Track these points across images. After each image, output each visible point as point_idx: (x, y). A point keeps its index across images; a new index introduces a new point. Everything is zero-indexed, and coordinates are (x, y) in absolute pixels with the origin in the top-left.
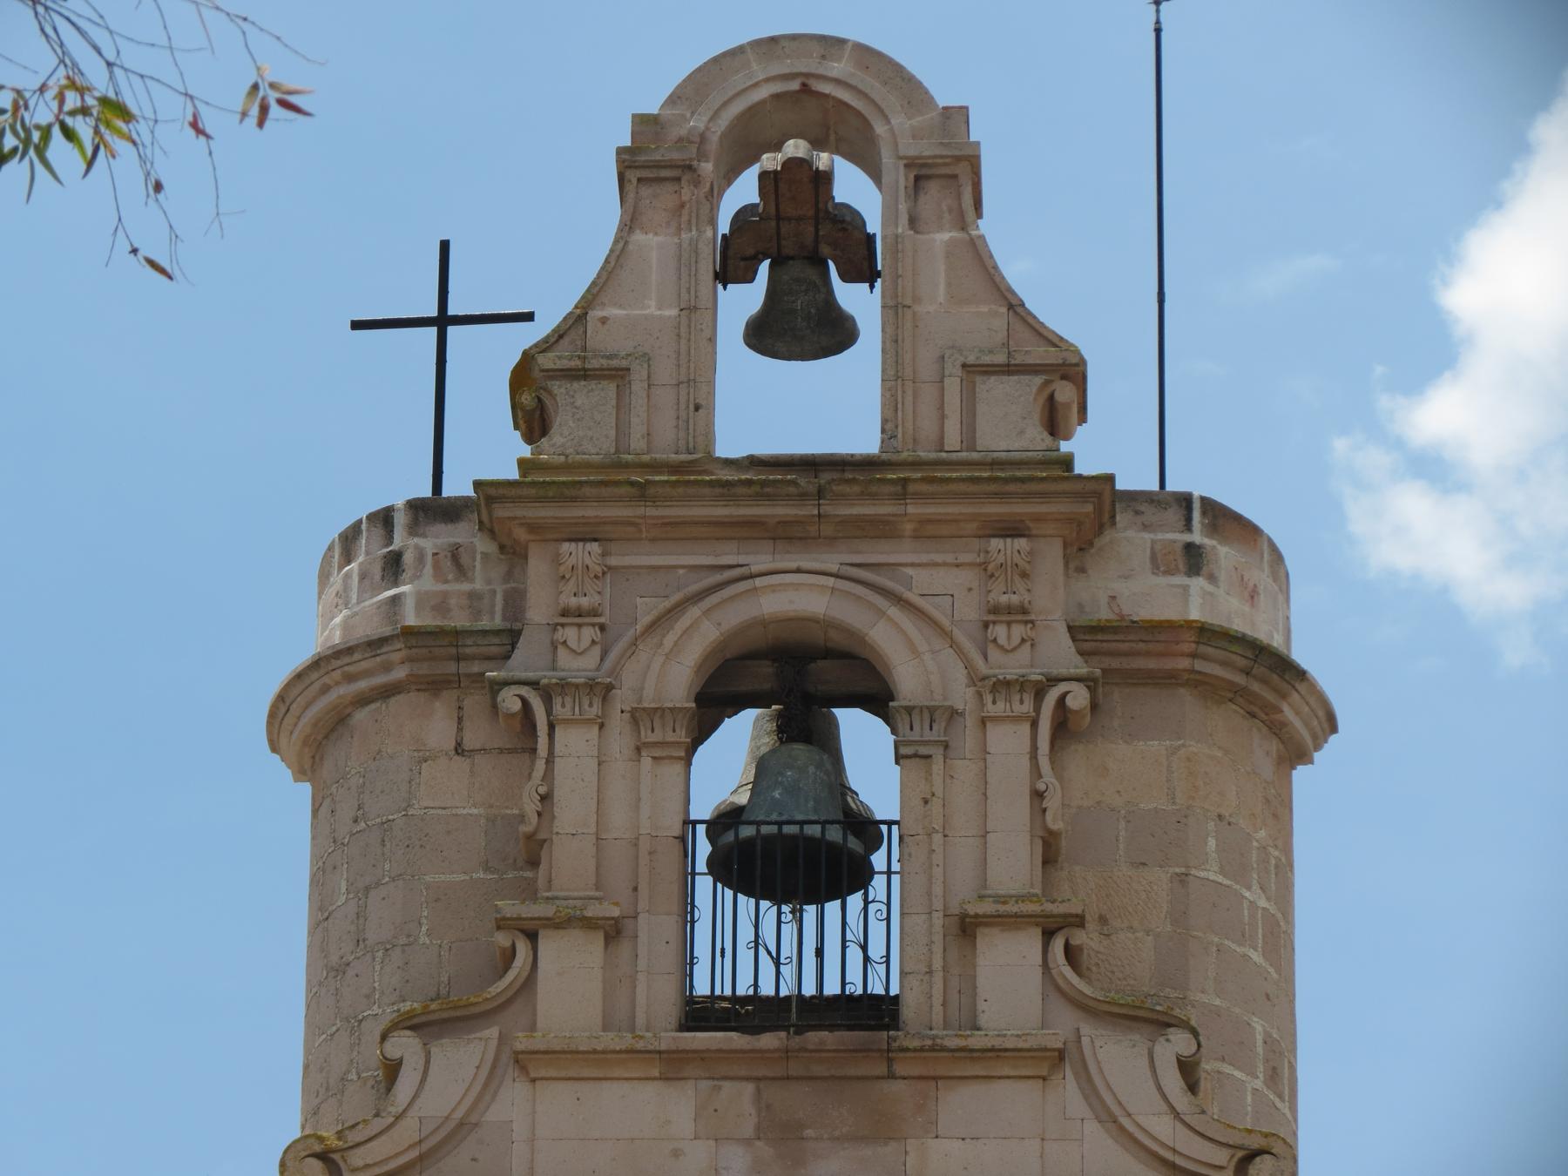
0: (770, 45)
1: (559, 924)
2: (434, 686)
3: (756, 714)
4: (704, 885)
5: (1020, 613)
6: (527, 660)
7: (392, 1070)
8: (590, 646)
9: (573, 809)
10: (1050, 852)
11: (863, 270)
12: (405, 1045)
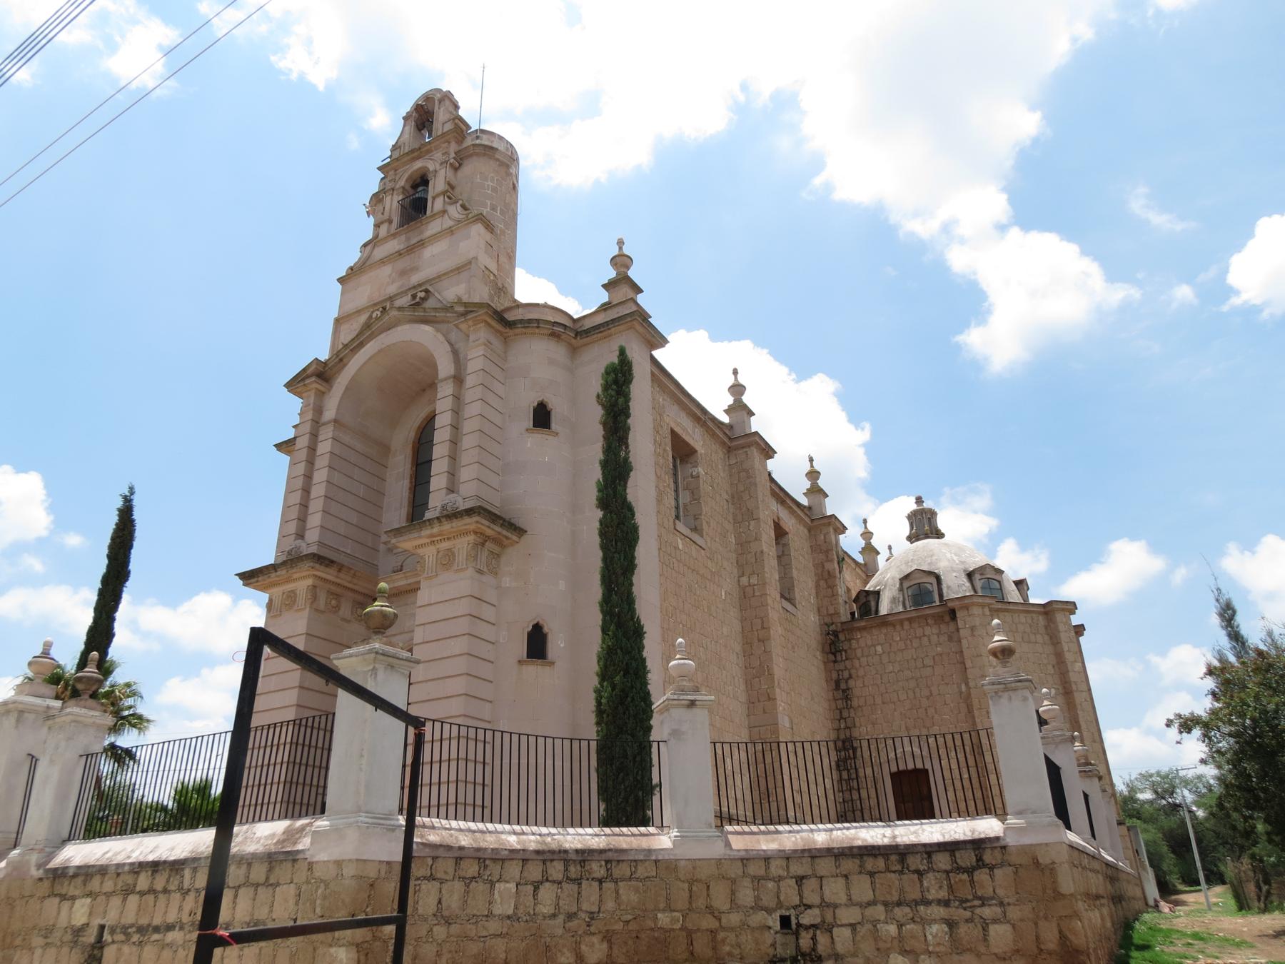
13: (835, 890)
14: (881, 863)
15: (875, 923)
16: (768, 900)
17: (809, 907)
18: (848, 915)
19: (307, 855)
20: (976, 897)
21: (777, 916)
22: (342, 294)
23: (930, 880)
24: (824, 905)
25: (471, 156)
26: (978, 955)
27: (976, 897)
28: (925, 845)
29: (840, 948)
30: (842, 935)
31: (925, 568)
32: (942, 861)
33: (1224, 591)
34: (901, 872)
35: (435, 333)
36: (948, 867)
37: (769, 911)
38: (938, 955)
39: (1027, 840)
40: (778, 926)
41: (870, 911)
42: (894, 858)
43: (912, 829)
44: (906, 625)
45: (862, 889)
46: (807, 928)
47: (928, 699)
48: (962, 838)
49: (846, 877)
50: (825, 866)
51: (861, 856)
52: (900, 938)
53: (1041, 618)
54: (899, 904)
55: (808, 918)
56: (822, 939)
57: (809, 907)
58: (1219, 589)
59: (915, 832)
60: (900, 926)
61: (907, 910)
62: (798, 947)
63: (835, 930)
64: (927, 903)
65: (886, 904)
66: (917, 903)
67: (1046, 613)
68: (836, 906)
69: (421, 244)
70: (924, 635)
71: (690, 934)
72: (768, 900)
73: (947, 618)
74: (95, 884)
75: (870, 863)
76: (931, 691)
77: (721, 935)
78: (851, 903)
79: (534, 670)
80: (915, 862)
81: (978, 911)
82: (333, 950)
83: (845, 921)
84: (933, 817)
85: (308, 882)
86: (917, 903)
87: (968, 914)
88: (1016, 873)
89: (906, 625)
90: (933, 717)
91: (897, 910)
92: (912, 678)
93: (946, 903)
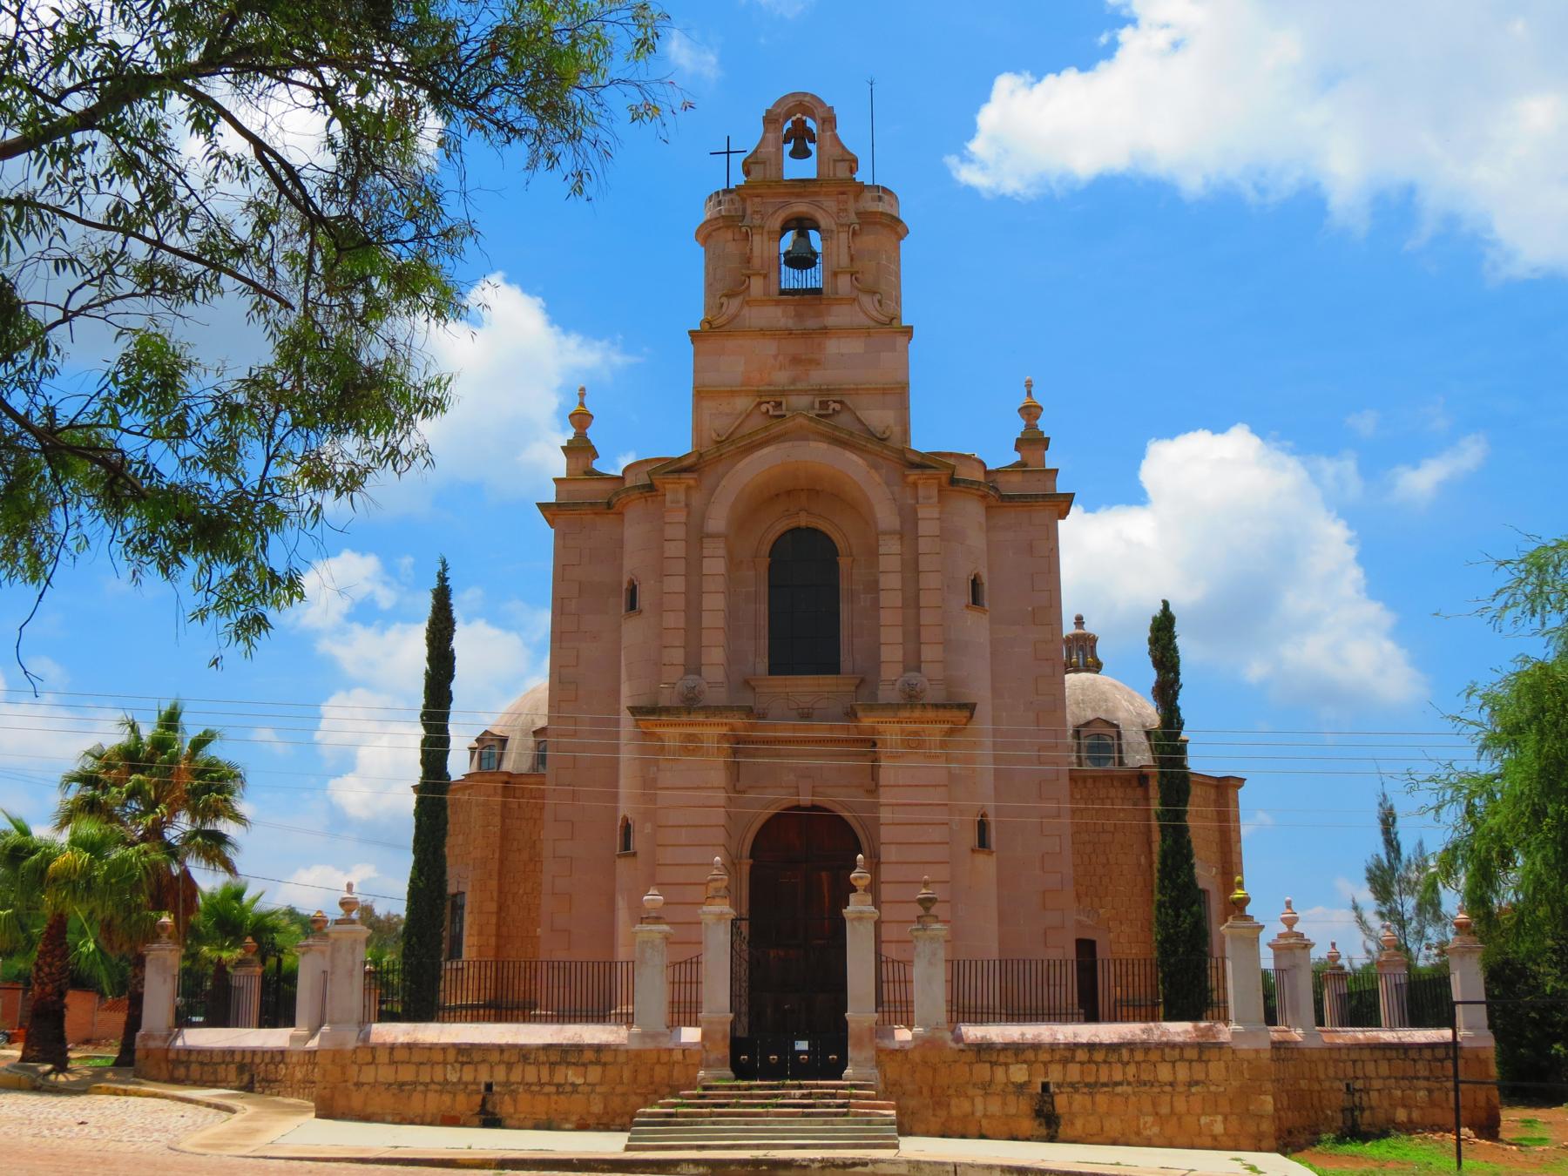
2: (728, 227)
6: (747, 221)
9: (757, 252)
11: (813, 141)
12: (724, 300)
13: (1370, 1069)
14: (1394, 1054)
15: (1390, 1089)
16: (1341, 1075)
17: (1357, 1078)
18: (1377, 1084)
19: (1231, 1045)
20: (1444, 1076)
21: (1344, 1083)
22: (696, 354)
23: (1420, 1065)
24: (1366, 1077)
25: (875, 223)
26: (1442, 1108)
27: (1444, 1076)
28: (1418, 1044)
29: (1374, 1103)
30: (1374, 1095)
31: (1103, 716)
32: (1427, 1054)
33: (1389, 797)
34: (1404, 1060)
35: (868, 469)
36: (1430, 1058)
37: (1341, 1080)
38: (1422, 1108)
39: (1475, 1045)
40: (1345, 1089)
41: (1387, 1082)
42: (1401, 1051)
43: (1408, 1033)
44: (1090, 783)
45: (1384, 1069)
46: (1358, 1091)
47: (1104, 867)
48: (1437, 1041)
49: (1375, 1061)
50: (1366, 1054)
51: (1384, 1049)
52: (1403, 1098)
53: (1213, 791)
54: (1403, 1078)
55: (1359, 1084)
56: (1365, 1098)
57: (1357, 1078)
58: (1384, 795)
59: (1409, 1036)
60: (1403, 1091)
61: (1407, 1082)
62: (1353, 1102)
63: (1371, 1093)
64: (1418, 1078)
65: (1395, 1078)
66: (1412, 1078)
67: (1217, 787)
68: (1371, 1078)
69: (825, 331)
70: (1108, 798)
71: (1311, 1092)
72: (1341, 1075)
73: (1135, 783)
74: (1030, 1055)
75: (1389, 1054)
76: (1108, 859)
77: (1322, 1094)
78: (1378, 1077)
79: (981, 858)
80: (1413, 1054)
81: (1445, 1084)
82: (1262, 1097)
83: (1376, 1088)
84: (1380, 1026)
85: (1233, 1060)
86: (1412, 1078)
87: (1438, 1085)
88: (1466, 1063)
89: (1090, 783)
90: (1107, 887)
91: (1401, 1082)
92: (1089, 842)
93: (1427, 1079)
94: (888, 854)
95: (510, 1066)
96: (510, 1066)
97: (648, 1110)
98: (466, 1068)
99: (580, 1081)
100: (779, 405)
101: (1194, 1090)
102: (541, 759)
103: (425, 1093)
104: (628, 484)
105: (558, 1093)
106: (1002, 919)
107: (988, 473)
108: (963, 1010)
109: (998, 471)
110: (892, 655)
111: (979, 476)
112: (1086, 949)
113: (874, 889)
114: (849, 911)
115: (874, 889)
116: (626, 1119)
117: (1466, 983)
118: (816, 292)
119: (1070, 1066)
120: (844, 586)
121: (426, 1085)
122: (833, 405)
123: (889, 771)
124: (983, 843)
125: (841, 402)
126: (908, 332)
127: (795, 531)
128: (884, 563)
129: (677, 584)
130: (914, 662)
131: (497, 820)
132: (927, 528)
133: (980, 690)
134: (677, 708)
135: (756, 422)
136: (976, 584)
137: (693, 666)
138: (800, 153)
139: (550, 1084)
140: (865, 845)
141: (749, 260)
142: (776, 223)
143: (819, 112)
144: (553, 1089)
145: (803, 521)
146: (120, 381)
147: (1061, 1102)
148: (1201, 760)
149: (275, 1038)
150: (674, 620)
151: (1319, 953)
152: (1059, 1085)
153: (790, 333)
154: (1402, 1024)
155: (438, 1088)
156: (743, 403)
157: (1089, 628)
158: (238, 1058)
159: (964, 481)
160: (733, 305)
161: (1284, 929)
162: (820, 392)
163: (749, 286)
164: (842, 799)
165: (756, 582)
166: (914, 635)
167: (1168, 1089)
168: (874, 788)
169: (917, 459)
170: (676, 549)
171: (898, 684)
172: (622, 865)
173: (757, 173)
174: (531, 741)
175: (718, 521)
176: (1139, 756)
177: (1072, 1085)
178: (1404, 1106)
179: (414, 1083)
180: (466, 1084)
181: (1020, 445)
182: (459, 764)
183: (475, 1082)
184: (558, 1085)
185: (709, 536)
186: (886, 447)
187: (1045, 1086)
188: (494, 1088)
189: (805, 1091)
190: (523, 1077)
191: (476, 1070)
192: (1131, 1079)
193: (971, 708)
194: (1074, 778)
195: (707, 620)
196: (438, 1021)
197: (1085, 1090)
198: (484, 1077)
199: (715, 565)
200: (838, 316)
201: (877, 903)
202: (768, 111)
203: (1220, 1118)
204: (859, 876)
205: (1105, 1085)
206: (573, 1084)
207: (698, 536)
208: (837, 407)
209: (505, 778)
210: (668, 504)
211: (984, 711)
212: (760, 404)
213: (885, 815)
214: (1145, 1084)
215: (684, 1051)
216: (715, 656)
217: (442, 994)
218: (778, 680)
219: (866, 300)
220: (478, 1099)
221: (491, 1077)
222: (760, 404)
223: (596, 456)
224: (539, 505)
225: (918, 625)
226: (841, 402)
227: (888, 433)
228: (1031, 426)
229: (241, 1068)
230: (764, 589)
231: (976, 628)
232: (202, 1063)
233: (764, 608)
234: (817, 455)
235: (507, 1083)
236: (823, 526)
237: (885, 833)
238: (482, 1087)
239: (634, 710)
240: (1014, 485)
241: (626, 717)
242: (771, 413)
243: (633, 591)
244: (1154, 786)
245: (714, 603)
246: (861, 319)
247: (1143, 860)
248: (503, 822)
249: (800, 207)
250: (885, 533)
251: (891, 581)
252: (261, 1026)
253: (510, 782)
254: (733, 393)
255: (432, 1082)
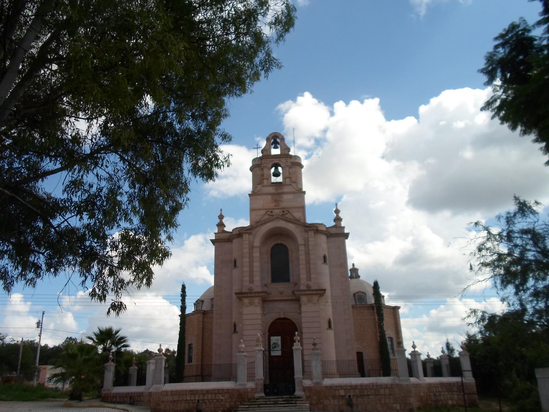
0: (274, 133)
1: (265, 179)
2: (258, 167)
3: (371, 284)
4: (272, 176)
5: (288, 162)
6: (262, 165)
7: (257, 187)
8: (221, 213)
9: (265, 173)
10: (290, 174)
11: (279, 144)
12: (257, 186)
69: (283, 193)
89: (358, 308)
93: (457, 392)
94: (304, 330)
95: (204, 395)
96: (204, 395)
97: (242, 406)
98: (192, 396)
99: (223, 398)
100: (272, 212)
101: (391, 396)
102: (212, 306)
103: (181, 403)
104: (233, 234)
105: (217, 402)
106: (336, 349)
107: (327, 228)
108: (326, 375)
109: (330, 227)
110: (303, 276)
111: (324, 229)
112: (360, 355)
113: (301, 341)
114: (294, 348)
115: (301, 341)
116: (236, 409)
117: (466, 365)
118: (280, 183)
119: (356, 390)
120: (290, 258)
121: (181, 401)
122: (286, 212)
123: (303, 308)
124: (330, 327)
125: (288, 211)
126: (304, 193)
127: (277, 244)
128: (300, 253)
129: (246, 260)
130: (309, 278)
131: (201, 323)
132: (311, 243)
133: (327, 285)
134: (247, 293)
135: (266, 217)
136: (325, 257)
137: (252, 281)
138: (276, 147)
139: (215, 399)
140: (299, 329)
141: (263, 175)
142: (270, 166)
143: (280, 137)
144: (216, 401)
145: (279, 242)
146: (171, 108)
147: (354, 401)
148: (388, 302)
149: (140, 389)
150: (246, 269)
151: (423, 357)
152: (353, 396)
153: (274, 194)
154: (449, 376)
155: (185, 402)
156: (263, 212)
157: (356, 267)
158: (130, 395)
159: (321, 230)
160: (259, 187)
161: (413, 350)
162: (282, 208)
163: (263, 182)
164: (291, 316)
165: (267, 258)
166: (309, 272)
167: (384, 396)
168: (300, 313)
169: (308, 225)
170: (246, 250)
171: (305, 285)
172: (235, 336)
173: (265, 153)
174: (210, 301)
175: (257, 243)
176: (371, 300)
177: (357, 396)
178: (451, 400)
179: (178, 401)
180: (192, 400)
181: (335, 220)
182: (190, 309)
183: (195, 400)
184: (217, 400)
185: (255, 247)
186: (300, 222)
187: (350, 396)
188: (200, 401)
189: (284, 399)
190: (208, 398)
191: (195, 396)
192: (373, 394)
193: (325, 290)
194: (353, 307)
195: (255, 269)
196: (184, 382)
197: (361, 397)
198: (197, 398)
199: (256, 254)
200: (286, 189)
201: (302, 345)
202: (267, 137)
203: (398, 405)
204: (297, 338)
205: (366, 396)
206: (221, 399)
207: (252, 247)
208: (287, 212)
209: (203, 312)
210: (244, 239)
211: (328, 293)
212: (267, 212)
213: (303, 320)
214: (377, 395)
215: (254, 362)
216: (257, 278)
217: (185, 370)
218: (274, 284)
219: (294, 185)
220: (195, 404)
221: (199, 398)
222: (267, 212)
223: (225, 226)
224: (211, 240)
225: (310, 268)
226: (288, 211)
227: (300, 219)
228: (337, 216)
229: (131, 398)
230: (269, 259)
231: (325, 269)
232: (120, 397)
233: (269, 265)
234: (282, 224)
235: (203, 400)
236: (284, 243)
237: (304, 325)
238: (197, 401)
239: (236, 294)
240: (334, 231)
241: (234, 295)
242: (270, 214)
243: (235, 261)
244: (375, 308)
245: (257, 264)
246: (293, 190)
247: (374, 330)
248: (203, 324)
249: (276, 161)
250: (300, 245)
251: (302, 257)
252: (137, 385)
253: (204, 313)
254: (260, 209)
255: (183, 400)
